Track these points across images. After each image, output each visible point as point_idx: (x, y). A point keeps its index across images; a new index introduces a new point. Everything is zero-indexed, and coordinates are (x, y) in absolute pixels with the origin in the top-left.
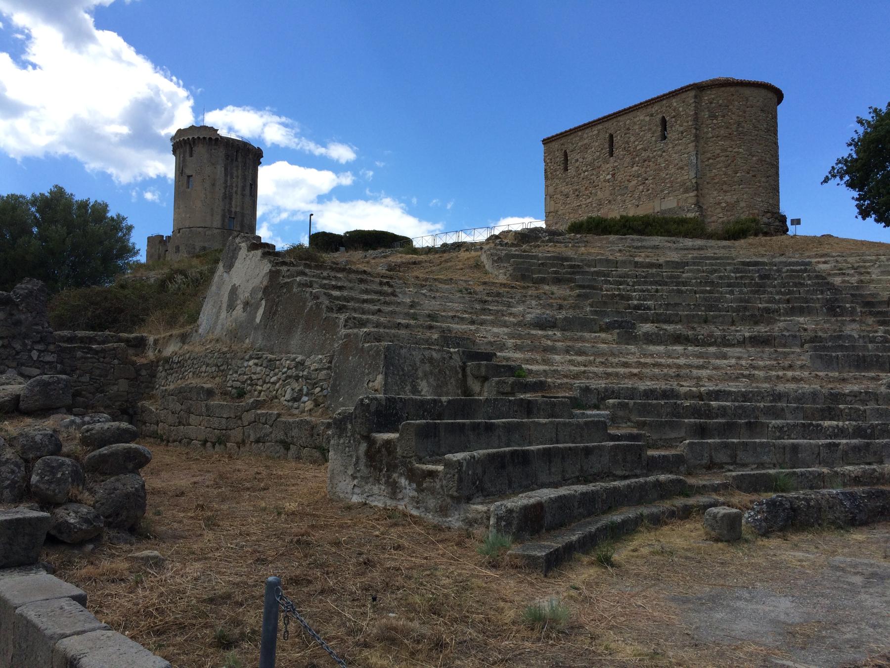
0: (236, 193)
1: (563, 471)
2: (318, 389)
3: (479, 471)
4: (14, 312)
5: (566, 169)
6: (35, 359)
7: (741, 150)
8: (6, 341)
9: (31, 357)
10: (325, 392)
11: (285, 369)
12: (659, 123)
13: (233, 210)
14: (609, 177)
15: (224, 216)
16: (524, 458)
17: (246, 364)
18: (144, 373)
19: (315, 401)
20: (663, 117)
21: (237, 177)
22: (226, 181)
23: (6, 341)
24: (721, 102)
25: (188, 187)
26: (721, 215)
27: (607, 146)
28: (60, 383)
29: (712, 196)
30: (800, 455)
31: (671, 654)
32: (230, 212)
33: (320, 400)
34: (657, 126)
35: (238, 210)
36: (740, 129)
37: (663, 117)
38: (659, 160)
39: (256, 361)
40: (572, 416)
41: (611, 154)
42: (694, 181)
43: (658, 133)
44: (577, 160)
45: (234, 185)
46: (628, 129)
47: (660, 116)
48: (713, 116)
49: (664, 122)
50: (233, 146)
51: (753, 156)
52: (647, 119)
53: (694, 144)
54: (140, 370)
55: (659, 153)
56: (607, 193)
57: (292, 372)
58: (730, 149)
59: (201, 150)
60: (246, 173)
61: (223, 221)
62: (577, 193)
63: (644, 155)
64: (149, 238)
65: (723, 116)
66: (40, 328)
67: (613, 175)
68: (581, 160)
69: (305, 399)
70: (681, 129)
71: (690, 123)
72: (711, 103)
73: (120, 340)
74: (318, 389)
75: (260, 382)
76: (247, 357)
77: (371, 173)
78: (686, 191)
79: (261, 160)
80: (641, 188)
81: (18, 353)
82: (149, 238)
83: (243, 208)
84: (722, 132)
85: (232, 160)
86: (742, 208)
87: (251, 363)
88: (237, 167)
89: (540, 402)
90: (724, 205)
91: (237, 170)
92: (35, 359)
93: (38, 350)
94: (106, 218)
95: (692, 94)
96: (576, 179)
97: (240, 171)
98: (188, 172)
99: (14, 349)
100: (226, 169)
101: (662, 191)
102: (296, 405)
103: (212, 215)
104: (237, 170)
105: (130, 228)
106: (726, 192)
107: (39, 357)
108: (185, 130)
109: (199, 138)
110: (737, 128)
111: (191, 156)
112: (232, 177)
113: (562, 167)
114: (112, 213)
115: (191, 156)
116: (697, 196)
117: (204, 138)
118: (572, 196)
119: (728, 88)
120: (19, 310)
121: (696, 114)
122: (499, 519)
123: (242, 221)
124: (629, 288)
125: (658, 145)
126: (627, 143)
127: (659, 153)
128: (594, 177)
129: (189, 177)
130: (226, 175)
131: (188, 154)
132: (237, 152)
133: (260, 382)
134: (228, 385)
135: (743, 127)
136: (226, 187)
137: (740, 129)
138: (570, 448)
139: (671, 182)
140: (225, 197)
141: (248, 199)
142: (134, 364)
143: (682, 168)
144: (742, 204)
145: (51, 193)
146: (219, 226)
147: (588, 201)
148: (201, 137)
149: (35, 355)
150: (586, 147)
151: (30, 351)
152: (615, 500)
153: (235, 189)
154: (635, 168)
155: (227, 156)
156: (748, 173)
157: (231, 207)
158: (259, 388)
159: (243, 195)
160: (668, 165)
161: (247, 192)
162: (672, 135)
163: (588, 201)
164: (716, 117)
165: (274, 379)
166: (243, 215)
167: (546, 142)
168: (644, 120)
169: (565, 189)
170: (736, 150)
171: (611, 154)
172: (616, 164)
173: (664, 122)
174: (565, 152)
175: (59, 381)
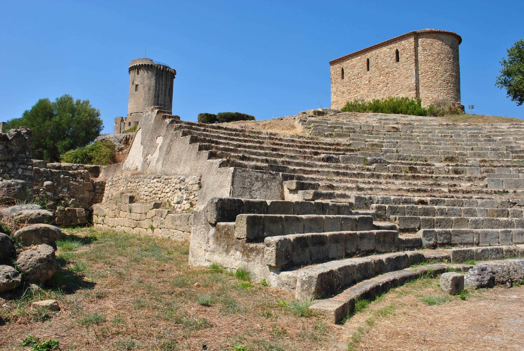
0: (161, 94)
1: (346, 249)
2: (193, 196)
3: (290, 248)
4: (8, 145)
5: (343, 78)
6: (20, 173)
7: (440, 68)
8: (3, 163)
9: (18, 172)
10: (197, 198)
11: (174, 185)
12: (395, 53)
14: (367, 82)
16: (320, 241)
17: (152, 181)
18: (98, 187)
19: (191, 203)
20: (397, 50)
23: (3, 163)
27: (366, 65)
28: (18, 185)
33: (194, 203)
34: (394, 54)
37: (397, 50)
38: (395, 73)
39: (158, 179)
40: (351, 214)
41: (368, 70)
43: (395, 58)
44: (349, 73)
46: (378, 56)
47: (395, 49)
49: (397, 52)
52: (388, 50)
54: (96, 185)
55: (395, 69)
56: (366, 91)
57: (178, 186)
58: (434, 68)
62: (349, 91)
63: (387, 70)
64: (115, 119)
66: (24, 155)
67: (369, 81)
68: (351, 73)
69: (185, 202)
70: (407, 56)
71: (412, 53)
73: (85, 168)
74: (193, 196)
75: (160, 192)
76: (153, 177)
78: (410, 91)
79: (175, 76)
80: (385, 88)
81: (10, 170)
83: (165, 102)
84: (429, 58)
87: (155, 180)
88: (162, 79)
89: (330, 205)
90: (431, 98)
92: (20, 173)
93: (22, 169)
94: (377, 295)
96: (348, 83)
98: (136, 83)
99: (8, 167)
101: (397, 90)
102: (179, 206)
105: (87, 102)
106: (432, 91)
107: (23, 172)
111: (138, 74)
112: (159, 85)
113: (341, 76)
115: (138, 74)
117: (145, 64)
118: (346, 93)
120: (11, 144)
121: (415, 48)
122: (303, 283)
124: (381, 140)
125: (394, 64)
126: (377, 63)
127: (395, 69)
128: (358, 82)
129: (137, 86)
133: (160, 192)
134: (142, 194)
138: (350, 234)
139: (402, 85)
141: (167, 97)
142: (93, 181)
143: (407, 78)
145: (78, 103)
147: (356, 95)
149: (20, 171)
150: (354, 66)
151: (17, 169)
152: (380, 268)
153: (161, 92)
154: (382, 77)
157: (158, 101)
158: (160, 196)
159: (165, 95)
160: (400, 76)
161: (167, 93)
163: (356, 95)
164: (426, 50)
165: (168, 190)
168: (385, 51)
169: (342, 89)
171: (368, 70)
172: (371, 75)
173: (397, 52)
174: (342, 68)
175: (18, 184)
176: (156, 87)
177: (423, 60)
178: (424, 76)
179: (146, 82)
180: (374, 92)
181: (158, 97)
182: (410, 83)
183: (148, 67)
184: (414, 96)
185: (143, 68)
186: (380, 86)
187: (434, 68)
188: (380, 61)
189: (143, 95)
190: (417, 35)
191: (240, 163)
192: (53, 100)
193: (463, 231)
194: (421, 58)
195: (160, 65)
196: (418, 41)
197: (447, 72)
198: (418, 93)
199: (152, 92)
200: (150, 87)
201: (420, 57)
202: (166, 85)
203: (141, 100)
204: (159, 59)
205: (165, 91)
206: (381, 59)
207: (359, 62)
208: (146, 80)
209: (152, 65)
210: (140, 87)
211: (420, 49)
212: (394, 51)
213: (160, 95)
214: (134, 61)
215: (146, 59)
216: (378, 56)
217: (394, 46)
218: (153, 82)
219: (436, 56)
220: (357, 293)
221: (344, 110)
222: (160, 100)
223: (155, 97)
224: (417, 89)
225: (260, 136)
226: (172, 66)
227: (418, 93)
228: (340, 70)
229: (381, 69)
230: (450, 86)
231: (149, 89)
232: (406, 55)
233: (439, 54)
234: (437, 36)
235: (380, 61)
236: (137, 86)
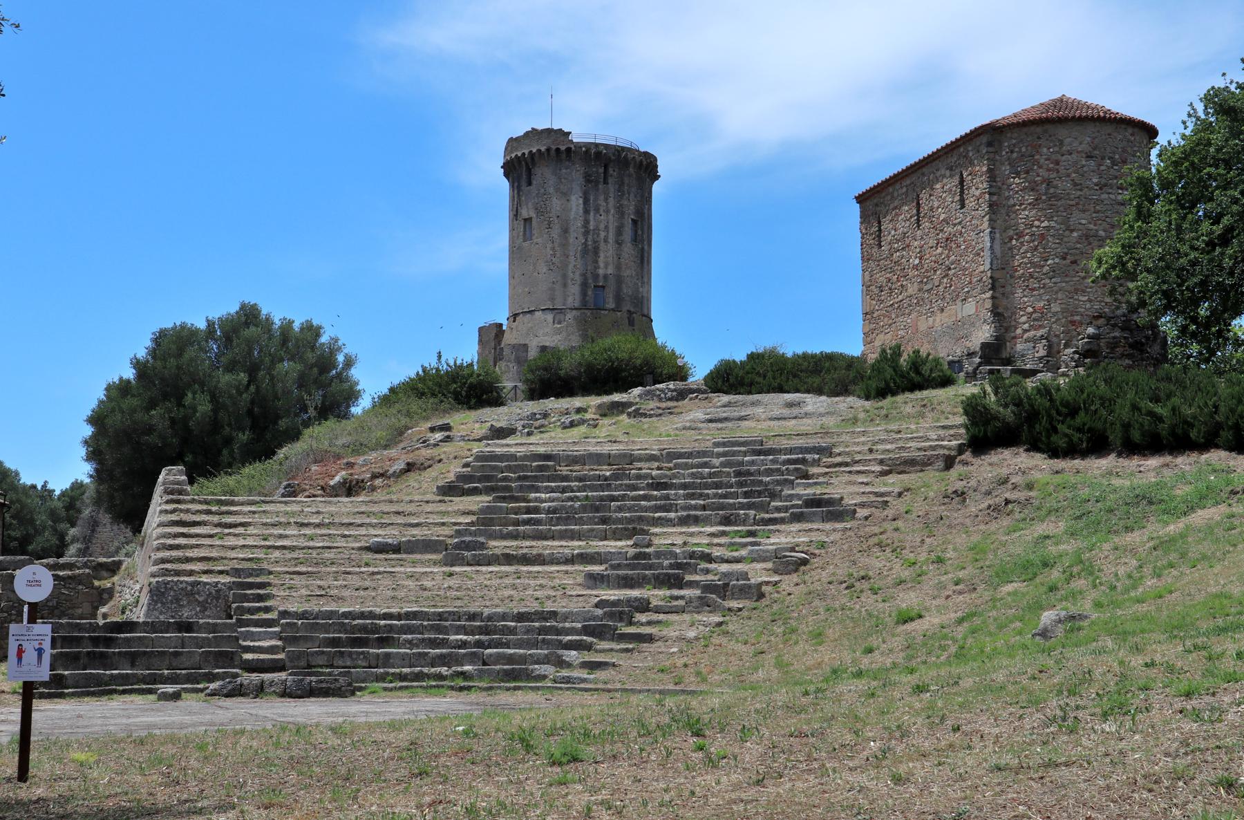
0: (606, 241)
7: (1053, 224)
13: (601, 272)
15: (584, 285)
21: (607, 212)
22: (587, 222)
24: (1024, 149)
30: (141, 620)
32: (596, 277)
35: (610, 271)
36: (1052, 190)
45: (602, 226)
50: (598, 154)
51: (1072, 231)
58: (1037, 223)
59: (544, 174)
61: (584, 294)
64: (481, 329)
65: (1027, 172)
72: (1012, 152)
82: (481, 329)
83: (618, 267)
85: (597, 183)
86: (1055, 314)
91: (606, 200)
95: (984, 139)
97: (611, 201)
98: (525, 213)
100: (586, 201)
103: (565, 285)
104: (606, 200)
106: (1033, 290)
108: (517, 139)
109: (539, 151)
110: (1047, 189)
114: (88, 431)
115: (530, 184)
119: (1032, 128)
129: (528, 221)
130: (586, 212)
131: (524, 183)
132: (606, 167)
135: (1056, 187)
137: (1052, 190)
140: (585, 251)
141: (628, 249)
146: (577, 305)
147: (900, 297)
148: (543, 149)
153: (603, 234)
154: (940, 250)
155: (588, 179)
156: (1064, 259)
159: (619, 243)
162: (970, 203)
166: (619, 280)
167: (861, 199)
170: (1046, 224)
182: (982, 268)
191: (632, 587)
192: (264, 312)
193: (619, 587)
202: (621, 212)
205: (619, 231)
213: (602, 244)
220: (404, 536)
232: (978, 187)
234: (1046, 131)
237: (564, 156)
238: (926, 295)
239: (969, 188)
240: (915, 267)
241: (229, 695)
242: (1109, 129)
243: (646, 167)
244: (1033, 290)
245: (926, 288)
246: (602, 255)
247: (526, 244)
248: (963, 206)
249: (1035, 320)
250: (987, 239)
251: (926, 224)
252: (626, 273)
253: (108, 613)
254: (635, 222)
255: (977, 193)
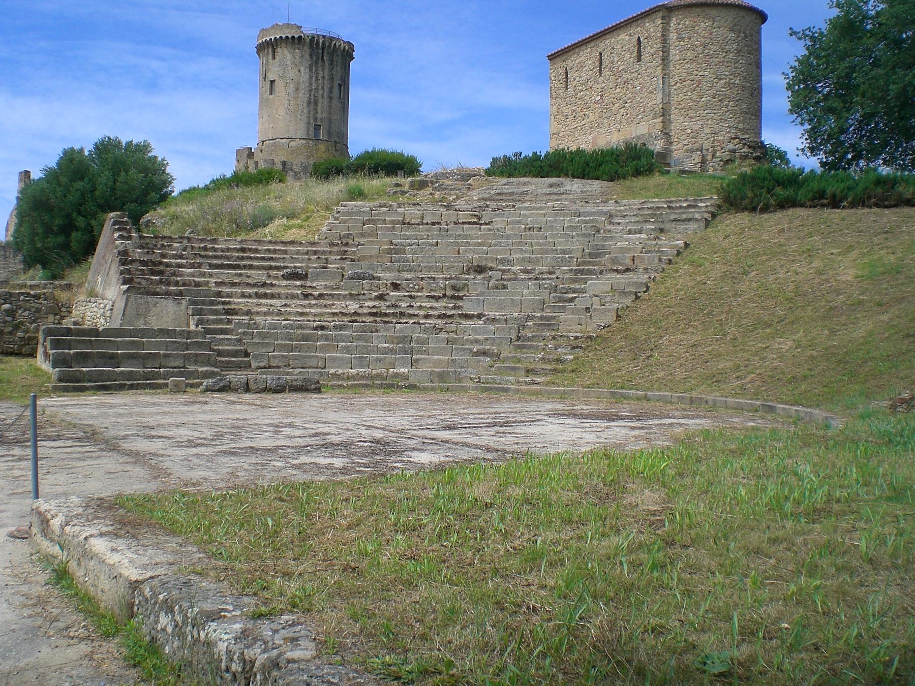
0: (323, 97)
14: (599, 98)
25: (271, 94)
26: (686, 142)
27: (597, 64)
29: (678, 122)
31: (595, 481)
37: (639, 38)
38: (637, 83)
42: (661, 106)
43: (635, 54)
48: (680, 39)
52: (627, 38)
53: (660, 67)
60: (334, 72)
63: (626, 76)
67: (601, 96)
68: (578, 79)
77: (869, 27)
78: (654, 118)
83: (330, 114)
84: (689, 54)
91: (323, 70)
97: (326, 71)
98: (271, 77)
104: (323, 70)
106: (691, 118)
109: (281, 37)
111: (274, 58)
115: (274, 58)
116: (663, 122)
121: (663, 35)
123: (330, 127)
129: (272, 82)
136: (311, 90)
137: (706, 51)
141: (336, 103)
144: (707, 130)
147: (583, 123)
148: (284, 36)
150: (581, 66)
153: (321, 92)
154: (618, 90)
159: (330, 98)
162: (646, 57)
164: (682, 39)
168: (623, 40)
169: (567, 110)
176: (311, 84)
177: (678, 57)
178: (679, 88)
179: (292, 73)
180: (608, 118)
181: (316, 103)
182: (655, 102)
183: (296, 41)
184: (659, 126)
185: (284, 45)
186: (616, 105)
187: (695, 73)
188: (616, 59)
189: (285, 102)
190: (668, 10)
194: (675, 55)
195: (318, 36)
196: (668, 24)
197: (720, 79)
198: (666, 123)
199: (303, 96)
200: (298, 83)
201: (674, 52)
202: (332, 79)
203: (282, 111)
204: (312, 25)
206: (619, 54)
207: (587, 57)
208: (290, 67)
209: (300, 37)
210: (279, 85)
211: (673, 36)
212: (635, 40)
213: (320, 100)
214: (264, 31)
215: (288, 25)
216: (613, 48)
217: (636, 31)
218: (305, 76)
219: (700, 49)
221: (489, 173)
222: (319, 111)
223: (309, 103)
224: (665, 113)
225: (216, 246)
226: (345, 34)
227: (666, 123)
228: (562, 71)
229: (617, 75)
230: (727, 106)
231: (297, 89)
232: (651, 49)
233: (705, 46)
235: (616, 59)
236: (272, 82)
237: (296, 41)
238: (606, 121)
239: (644, 48)
240: (596, 102)
241: (220, 390)
242: (742, 13)
243: (347, 54)
244: (691, 118)
245: (605, 116)
246: (320, 105)
247: (271, 97)
248: (639, 60)
249: (692, 138)
250: (660, 81)
251: (606, 72)
252: (334, 117)
253: (819, 170)
254: (340, 85)
255: (652, 51)
